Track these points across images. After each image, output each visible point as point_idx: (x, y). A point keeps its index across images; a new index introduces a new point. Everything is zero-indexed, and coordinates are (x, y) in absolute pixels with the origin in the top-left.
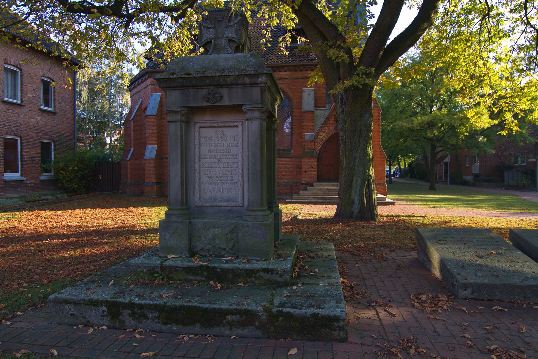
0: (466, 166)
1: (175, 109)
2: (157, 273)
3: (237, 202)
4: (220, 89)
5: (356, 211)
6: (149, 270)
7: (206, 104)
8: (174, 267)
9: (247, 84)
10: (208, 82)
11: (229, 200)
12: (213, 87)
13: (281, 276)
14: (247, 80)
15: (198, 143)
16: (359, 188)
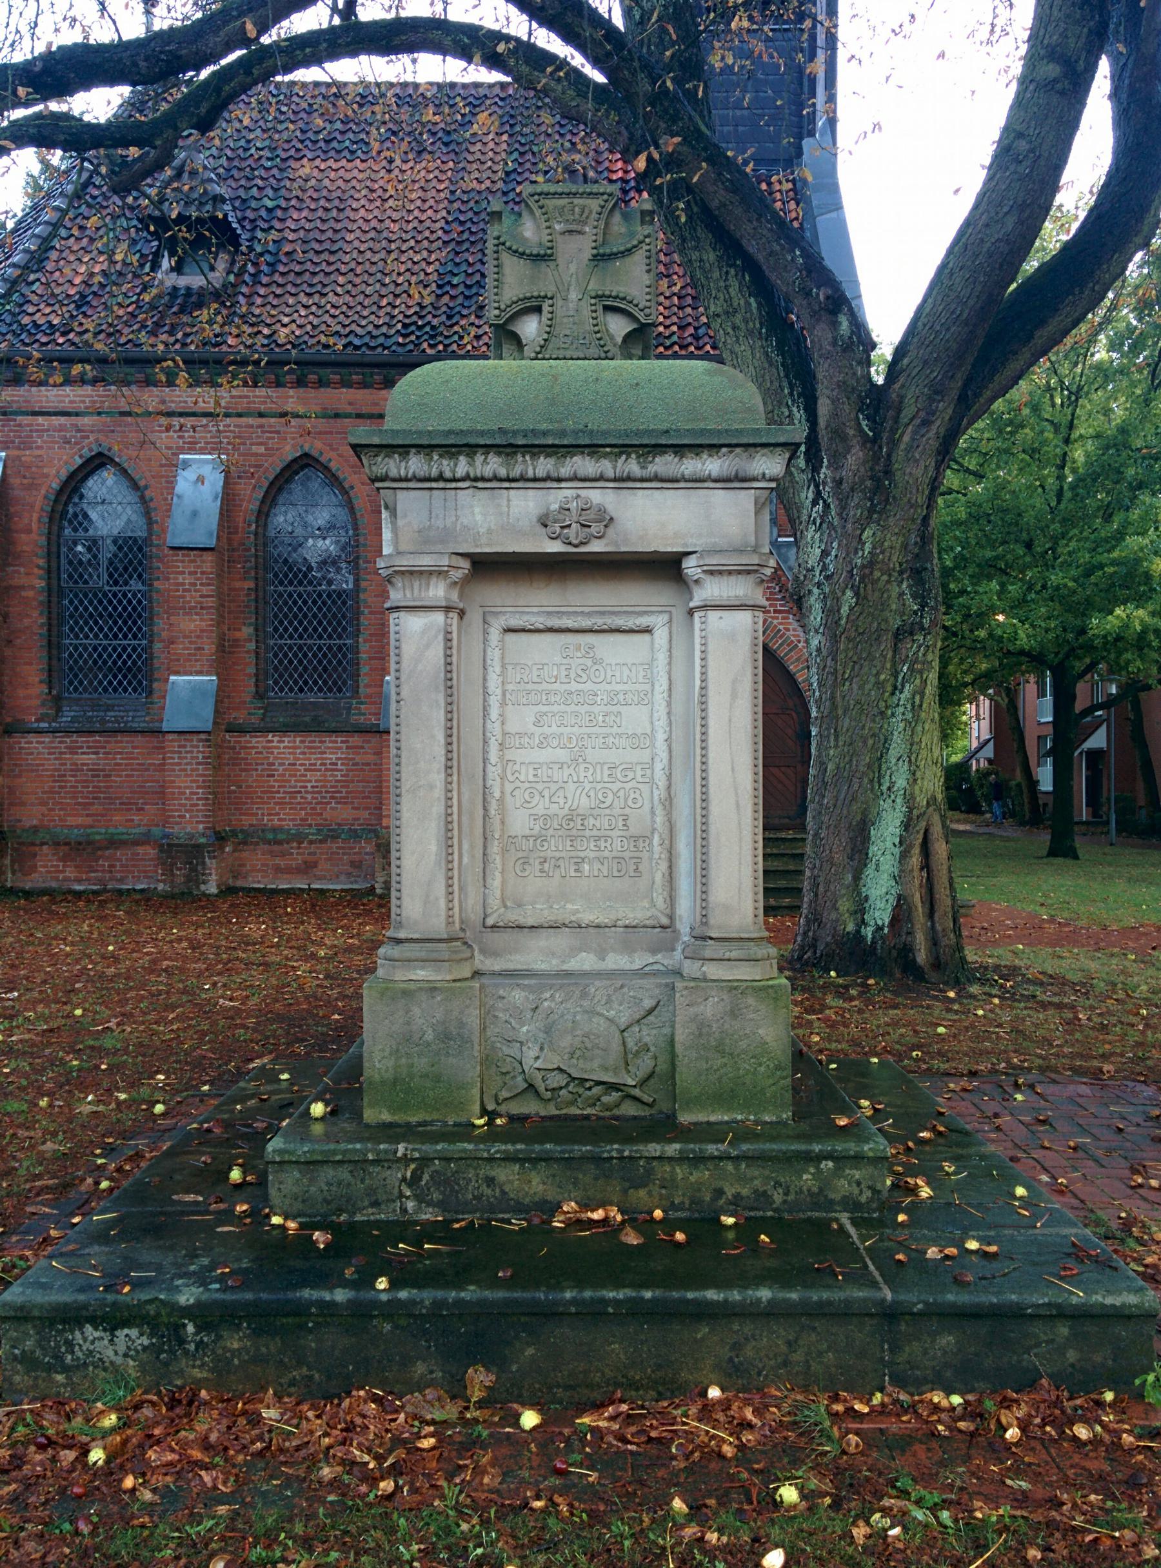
15: (499, 692)
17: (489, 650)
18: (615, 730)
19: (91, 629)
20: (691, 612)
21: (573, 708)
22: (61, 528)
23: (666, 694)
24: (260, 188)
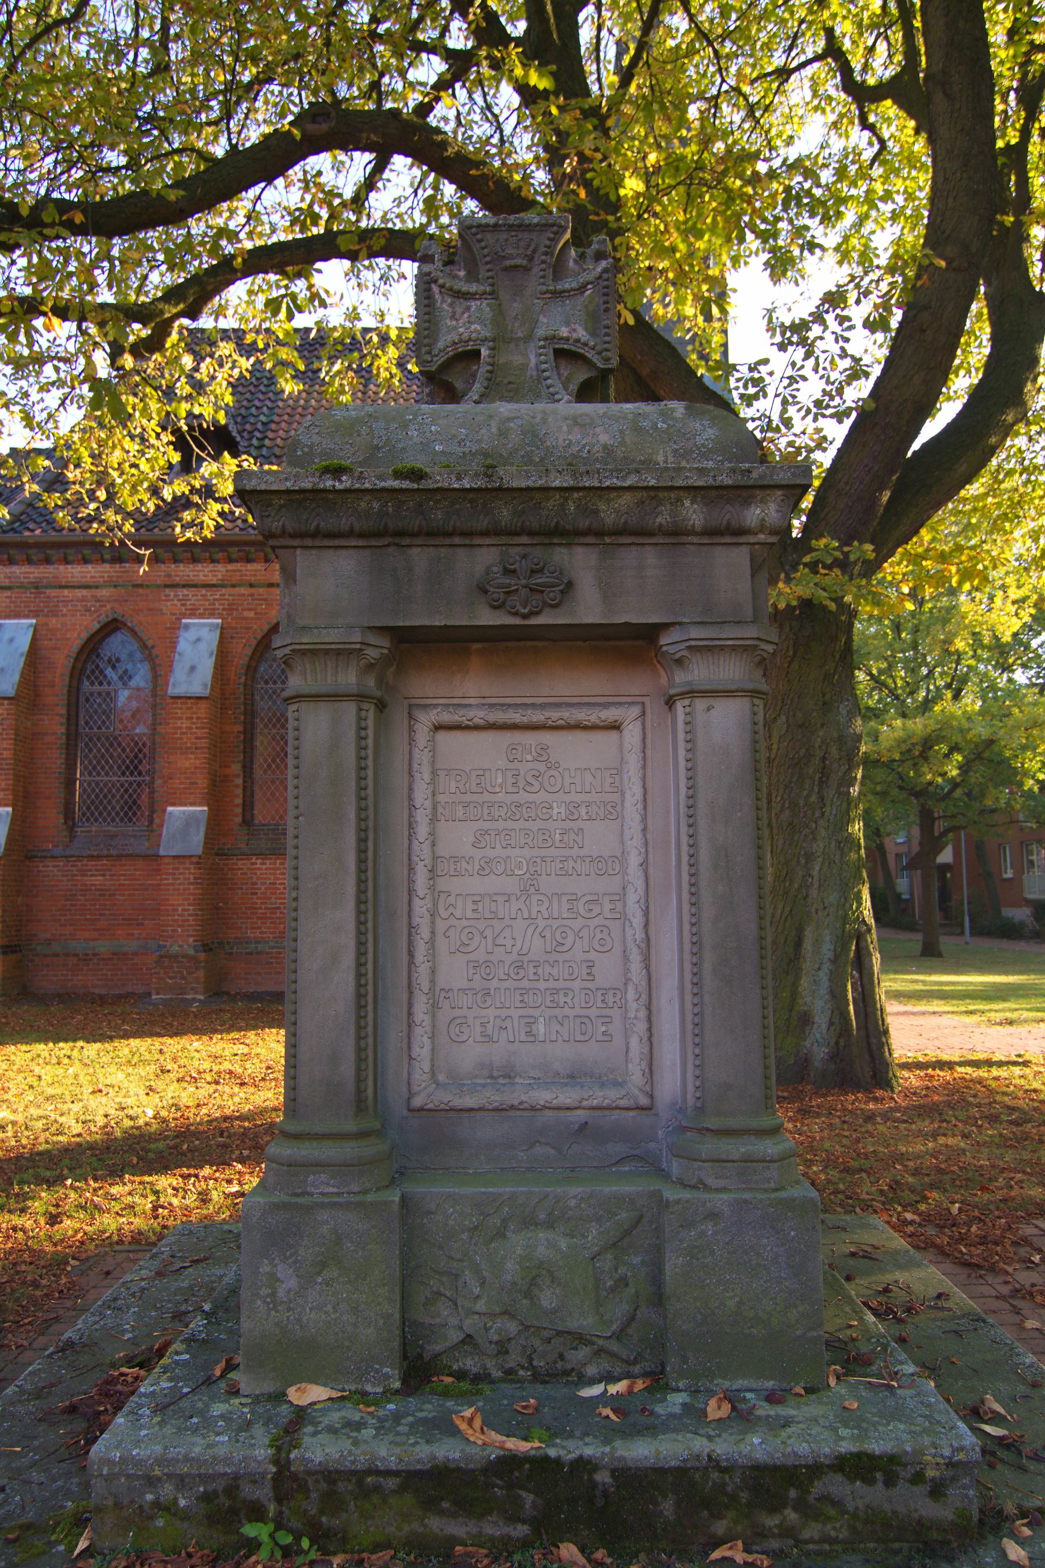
0: (1005, 876)
1: (333, 637)
2: (257, 1514)
3: (618, 1084)
4: (558, 550)
5: (820, 1053)
6: (207, 1498)
7: (488, 618)
8: (354, 1472)
9: (693, 532)
10: (504, 514)
11: (573, 1077)
12: (525, 539)
13: (937, 1491)
14: (694, 514)
15: (428, 804)
16: (827, 966)
17: (416, 752)
18: (575, 852)
19: (103, 768)
20: (670, 702)
21: (522, 824)
22: (80, 681)
23: (640, 806)
24: (257, 408)
